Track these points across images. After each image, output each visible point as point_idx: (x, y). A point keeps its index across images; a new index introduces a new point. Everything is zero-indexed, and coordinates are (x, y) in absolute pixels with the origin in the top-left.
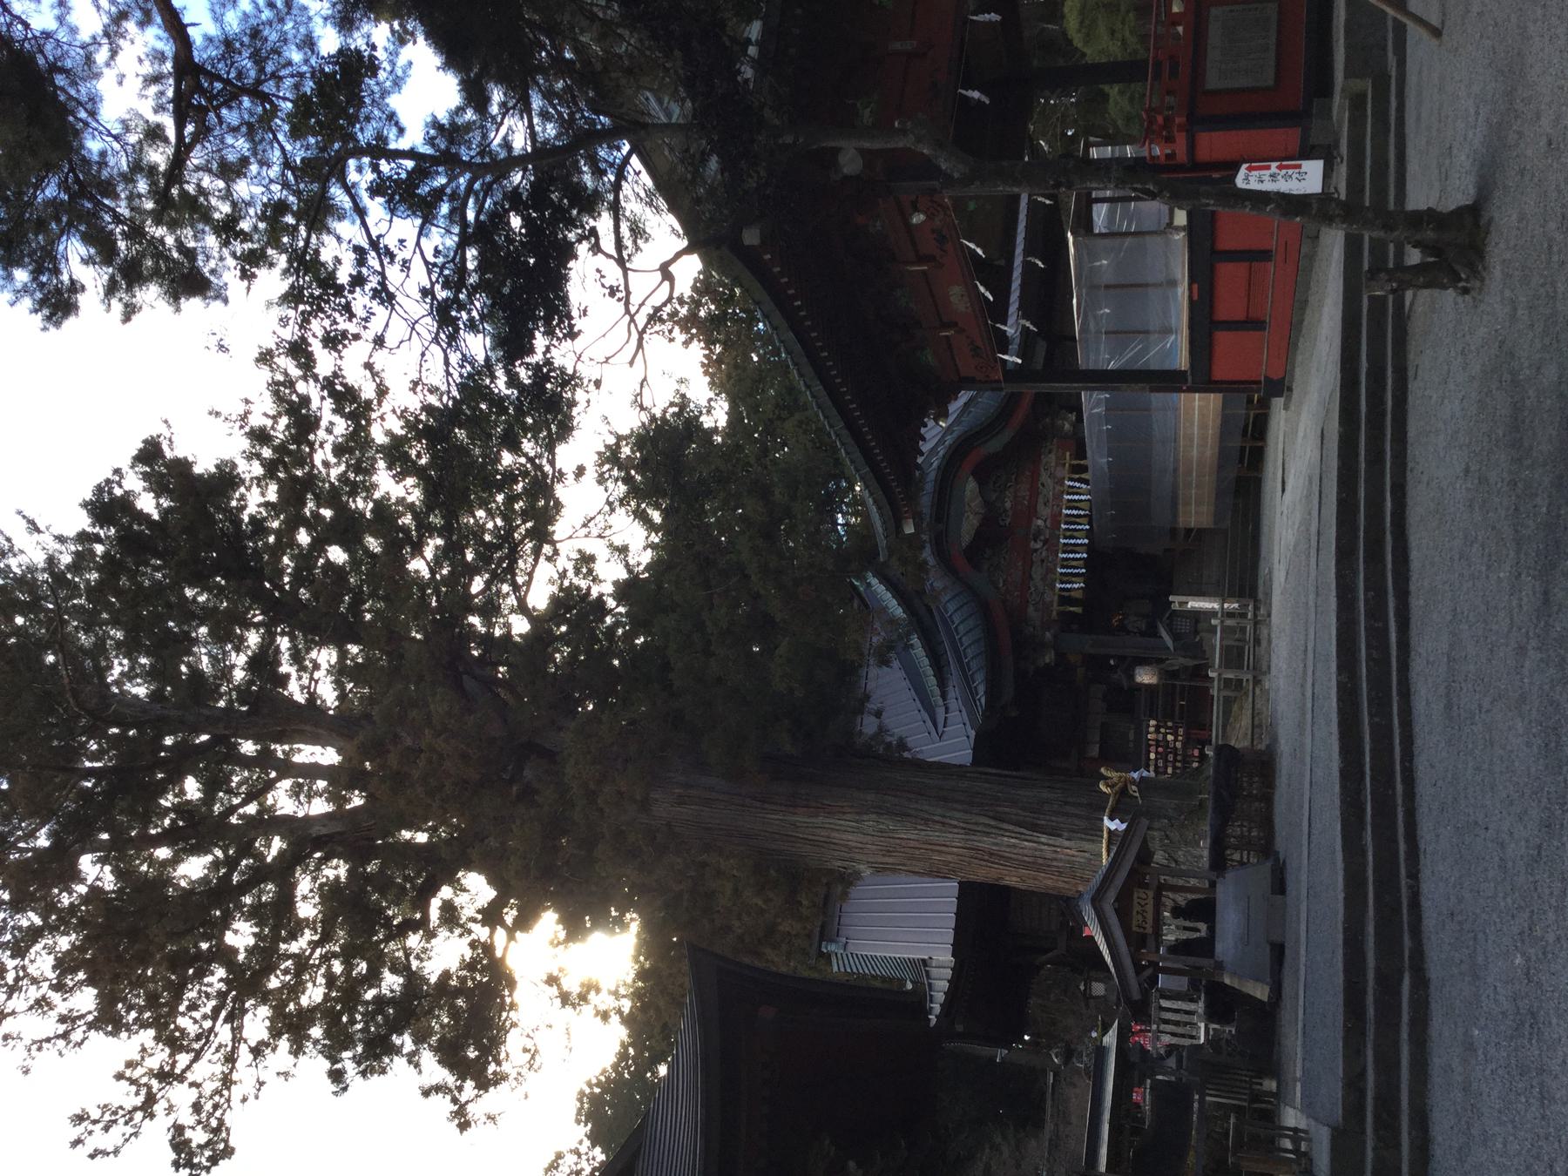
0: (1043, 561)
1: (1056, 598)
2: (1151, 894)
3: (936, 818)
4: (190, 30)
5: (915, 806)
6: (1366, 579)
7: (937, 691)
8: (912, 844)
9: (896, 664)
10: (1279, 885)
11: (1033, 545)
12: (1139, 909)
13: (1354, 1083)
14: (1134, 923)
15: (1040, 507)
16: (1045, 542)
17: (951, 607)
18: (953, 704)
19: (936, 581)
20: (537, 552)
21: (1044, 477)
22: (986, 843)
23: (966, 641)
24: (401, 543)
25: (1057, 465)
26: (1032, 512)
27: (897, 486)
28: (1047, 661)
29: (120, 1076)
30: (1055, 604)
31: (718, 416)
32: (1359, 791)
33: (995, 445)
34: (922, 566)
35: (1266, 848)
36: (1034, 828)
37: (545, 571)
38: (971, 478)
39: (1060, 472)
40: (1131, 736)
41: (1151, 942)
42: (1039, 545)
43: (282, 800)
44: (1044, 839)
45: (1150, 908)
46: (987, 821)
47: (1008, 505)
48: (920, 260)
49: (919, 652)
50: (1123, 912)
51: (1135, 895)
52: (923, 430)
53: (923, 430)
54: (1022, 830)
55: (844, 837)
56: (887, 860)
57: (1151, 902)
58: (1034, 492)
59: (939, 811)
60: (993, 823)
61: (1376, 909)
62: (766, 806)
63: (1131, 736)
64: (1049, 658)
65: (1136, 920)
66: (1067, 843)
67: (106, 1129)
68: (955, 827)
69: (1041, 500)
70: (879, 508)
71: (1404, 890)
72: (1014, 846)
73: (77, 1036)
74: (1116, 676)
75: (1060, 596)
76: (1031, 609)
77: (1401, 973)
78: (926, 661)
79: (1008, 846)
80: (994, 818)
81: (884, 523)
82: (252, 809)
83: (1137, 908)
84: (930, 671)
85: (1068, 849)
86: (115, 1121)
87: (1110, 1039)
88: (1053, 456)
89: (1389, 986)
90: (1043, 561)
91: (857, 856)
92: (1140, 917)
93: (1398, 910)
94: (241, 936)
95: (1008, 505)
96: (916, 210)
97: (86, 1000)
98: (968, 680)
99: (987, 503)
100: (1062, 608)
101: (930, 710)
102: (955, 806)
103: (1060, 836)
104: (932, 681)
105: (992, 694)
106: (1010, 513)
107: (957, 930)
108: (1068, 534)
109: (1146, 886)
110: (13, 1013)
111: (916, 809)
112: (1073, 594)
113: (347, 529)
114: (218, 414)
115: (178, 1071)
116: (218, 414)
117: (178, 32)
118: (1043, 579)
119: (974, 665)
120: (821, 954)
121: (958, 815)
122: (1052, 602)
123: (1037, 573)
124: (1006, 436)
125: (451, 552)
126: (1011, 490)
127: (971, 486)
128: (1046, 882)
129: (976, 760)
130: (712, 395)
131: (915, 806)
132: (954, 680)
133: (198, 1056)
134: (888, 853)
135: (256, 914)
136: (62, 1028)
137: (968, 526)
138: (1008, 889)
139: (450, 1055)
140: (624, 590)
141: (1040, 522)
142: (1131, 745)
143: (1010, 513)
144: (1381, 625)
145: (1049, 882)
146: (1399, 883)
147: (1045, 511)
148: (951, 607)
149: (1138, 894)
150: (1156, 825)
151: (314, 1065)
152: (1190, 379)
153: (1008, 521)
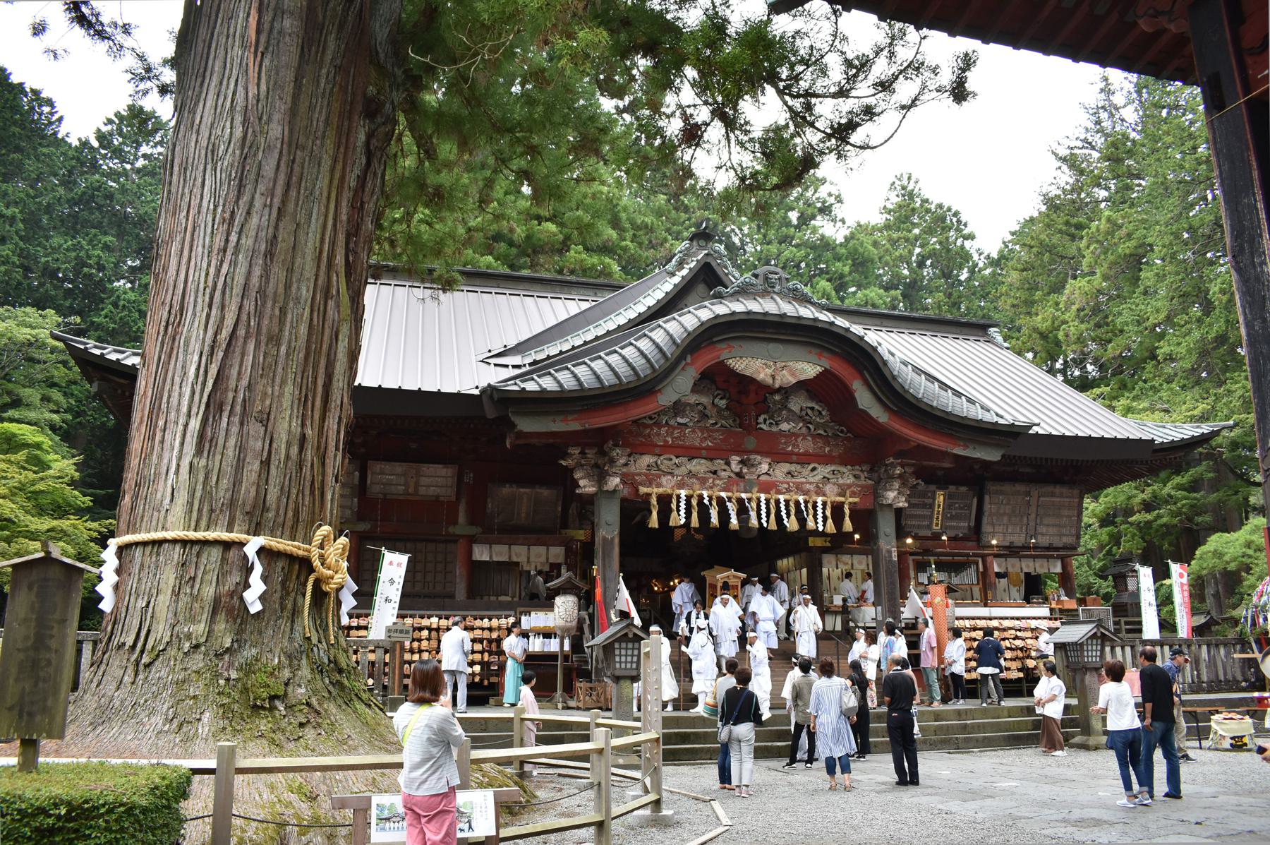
0: (715, 473)
1: (669, 491)
3: (234, 238)
8: (195, 203)
11: (735, 460)
15: (786, 467)
16: (740, 475)
21: (824, 471)
23: (598, 365)
26: (779, 457)
28: (582, 483)
30: (661, 490)
33: (864, 399)
38: (819, 369)
40: (502, 598)
42: (735, 467)
44: (195, 424)
47: (785, 426)
55: (211, 96)
59: (247, 242)
60: (225, 334)
64: (586, 486)
69: (793, 467)
75: (670, 496)
76: (647, 460)
78: (578, 342)
88: (851, 480)
90: (715, 473)
95: (785, 426)
99: (786, 391)
100: (654, 501)
102: (257, 271)
103: (199, 451)
106: (775, 429)
111: (251, 204)
112: (674, 514)
118: (690, 474)
119: (564, 377)
121: (241, 271)
122: (659, 485)
124: (878, 413)
126: (804, 430)
127: (809, 370)
131: (258, 203)
142: (493, 598)
147: (780, 472)
148: (644, 344)
153: (763, 426)
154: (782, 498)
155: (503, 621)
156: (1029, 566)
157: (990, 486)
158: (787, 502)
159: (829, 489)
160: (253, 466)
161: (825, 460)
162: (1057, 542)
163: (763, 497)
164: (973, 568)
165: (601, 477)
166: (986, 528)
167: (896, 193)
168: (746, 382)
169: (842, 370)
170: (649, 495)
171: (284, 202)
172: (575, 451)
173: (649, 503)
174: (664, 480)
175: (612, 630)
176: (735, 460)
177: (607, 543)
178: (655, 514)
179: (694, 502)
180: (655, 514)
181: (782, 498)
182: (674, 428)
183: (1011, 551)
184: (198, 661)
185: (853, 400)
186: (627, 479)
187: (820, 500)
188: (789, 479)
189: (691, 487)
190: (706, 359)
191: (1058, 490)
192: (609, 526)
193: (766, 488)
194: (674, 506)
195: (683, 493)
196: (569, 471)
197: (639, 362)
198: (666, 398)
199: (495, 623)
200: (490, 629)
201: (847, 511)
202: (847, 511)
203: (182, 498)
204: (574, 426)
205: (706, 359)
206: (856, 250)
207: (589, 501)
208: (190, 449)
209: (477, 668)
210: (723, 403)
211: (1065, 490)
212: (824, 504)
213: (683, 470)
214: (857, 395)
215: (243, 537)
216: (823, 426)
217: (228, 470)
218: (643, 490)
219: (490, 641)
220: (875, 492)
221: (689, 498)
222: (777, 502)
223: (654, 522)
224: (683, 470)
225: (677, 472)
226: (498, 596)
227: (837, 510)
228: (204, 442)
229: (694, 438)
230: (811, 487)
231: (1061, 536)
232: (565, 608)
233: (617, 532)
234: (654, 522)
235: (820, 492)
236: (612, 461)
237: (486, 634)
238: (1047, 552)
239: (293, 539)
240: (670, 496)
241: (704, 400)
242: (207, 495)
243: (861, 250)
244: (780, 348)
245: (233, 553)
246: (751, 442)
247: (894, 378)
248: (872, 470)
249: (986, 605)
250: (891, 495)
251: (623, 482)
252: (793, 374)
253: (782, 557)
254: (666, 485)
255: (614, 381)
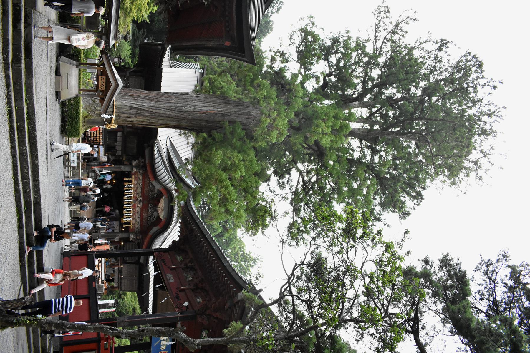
0: (138, 193)
2: (100, 88)
3: (169, 111)
4: (415, 344)
5: (176, 114)
6: (30, 195)
7: (170, 150)
8: (177, 102)
9: (183, 159)
10: (58, 94)
11: (141, 198)
12: (103, 84)
13: (28, 25)
14: (105, 79)
15: (139, 210)
16: (137, 199)
17: (166, 178)
18: (164, 146)
19: (172, 186)
20: (297, 189)
21: (139, 220)
22: (153, 104)
24: (337, 190)
25: (135, 224)
26: (142, 209)
27: (187, 216)
28: (135, 162)
29: (406, 32)
30: (133, 181)
31: (240, 232)
32: (29, 124)
33: (155, 229)
34: (176, 191)
35: (63, 105)
36: (138, 109)
37: (294, 183)
38: (162, 218)
39: (134, 222)
40: (108, 139)
41: (99, 73)
43: (364, 112)
44: (135, 106)
45: (100, 84)
46: (153, 111)
47: (150, 211)
48: (184, 290)
49: (177, 165)
50: (108, 83)
51: (105, 88)
52: (179, 234)
53: (179, 234)
54: (142, 108)
56: (184, 97)
57: (100, 86)
58: (141, 215)
59: (168, 113)
60: (151, 110)
61: (21, 83)
62: (223, 113)
63: (108, 139)
64: (134, 163)
65: (104, 80)
66: (128, 104)
67: (408, 17)
68: (163, 108)
69: (139, 213)
70: (192, 209)
71: (12, 91)
72: (144, 103)
73: (418, 43)
74: (113, 158)
75: (132, 183)
76: (141, 178)
77: (12, 61)
78: (173, 160)
79: (145, 103)
80: (151, 111)
81: (190, 204)
82: (374, 110)
83: (104, 84)
84: (172, 157)
85: (129, 102)
86: (406, 19)
87: (112, 42)
88: (136, 227)
89: (17, 59)
90: (138, 193)
91: (194, 98)
92: (103, 81)
93: (14, 83)
94: (375, 73)
95: (150, 211)
96: (187, 307)
97: (416, 53)
98: (160, 155)
99: (157, 211)
101: (172, 145)
104: (171, 153)
105: (153, 151)
106: (149, 208)
107: (161, 77)
108: (130, 203)
109: (102, 91)
110: (436, 50)
112: (127, 184)
113: (353, 193)
114: (388, 226)
115: (390, 34)
116: (388, 226)
117: (419, 343)
118: (137, 188)
120: (203, 69)
122: (134, 180)
123: (139, 190)
124: (151, 232)
125: (322, 188)
127: (162, 216)
128: (134, 92)
129: (157, 129)
130: (242, 239)
131: (176, 114)
132: (164, 154)
133: (385, 38)
134: (184, 99)
135: (372, 79)
136: (422, 46)
137: (162, 203)
138: (145, 89)
139: (316, 38)
140: (267, 179)
141: (139, 206)
142: (107, 137)
143: (149, 208)
144: (24, 181)
145: (132, 92)
146: (14, 93)
147: (138, 209)
149: (104, 89)
150: (509, 294)
151: (354, 36)
152: (94, 256)
154: (132, 209)
155: (101, 141)
156: (116, 277)
157: (137, 266)
158: (131, 211)
159: (134, 222)
160: (127, 115)
161: (141, 220)
162: (123, 285)
163: (132, 205)
164: (116, 262)
165: (137, 167)
166: (126, 265)
167: (257, 257)
168: (159, 201)
169: (162, 224)
170: (132, 178)
171: (176, 119)
172: (143, 160)
173: (130, 178)
174: (136, 181)
175: (98, 172)
176: (141, 198)
177: (120, 168)
178: (127, 179)
179: (130, 189)
180: (127, 179)
181: (132, 209)
182: (149, 184)
183: (120, 271)
184: (93, 108)
185: (155, 226)
186: (136, 173)
187: (131, 219)
188: (136, 211)
189: (134, 188)
190: (164, 192)
191: (137, 285)
192: (125, 168)
193: (134, 206)
194: (129, 184)
195: (133, 186)
196: (138, 159)
197: (162, 176)
198: (154, 183)
199: (101, 140)
200: (99, 138)
201: (128, 226)
202: (128, 226)
203: (121, 104)
204: (147, 162)
205: (164, 192)
206: (232, 241)
207: (131, 164)
208: (130, 105)
209: (89, 135)
210: (155, 196)
211: (137, 286)
212: (130, 220)
213: (138, 186)
214: (156, 227)
215: (114, 114)
216: (150, 220)
217: (126, 111)
218: (133, 177)
219: (96, 138)
220: (133, 232)
221: (131, 187)
222: (130, 208)
223: (125, 179)
224: (138, 186)
225: (138, 185)
226: (109, 138)
227: (128, 223)
228: (131, 108)
229: (146, 189)
230: (134, 217)
231: (124, 286)
232: (104, 159)
233: (123, 170)
234: (125, 179)
235: (133, 219)
236: (140, 169)
237: (98, 137)
238: (120, 283)
239: (116, 112)
240: (132, 183)
241: (156, 191)
242: (122, 109)
243: (232, 243)
244: (167, 209)
245: (111, 113)
246: (146, 202)
247: (159, 236)
248: (139, 232)
249: (105, 263)
250: (132, 236)
251: (135, 172)
252: (161, 212)
253: (119, 211)
254: (134, 182)
255: (157, 171)
